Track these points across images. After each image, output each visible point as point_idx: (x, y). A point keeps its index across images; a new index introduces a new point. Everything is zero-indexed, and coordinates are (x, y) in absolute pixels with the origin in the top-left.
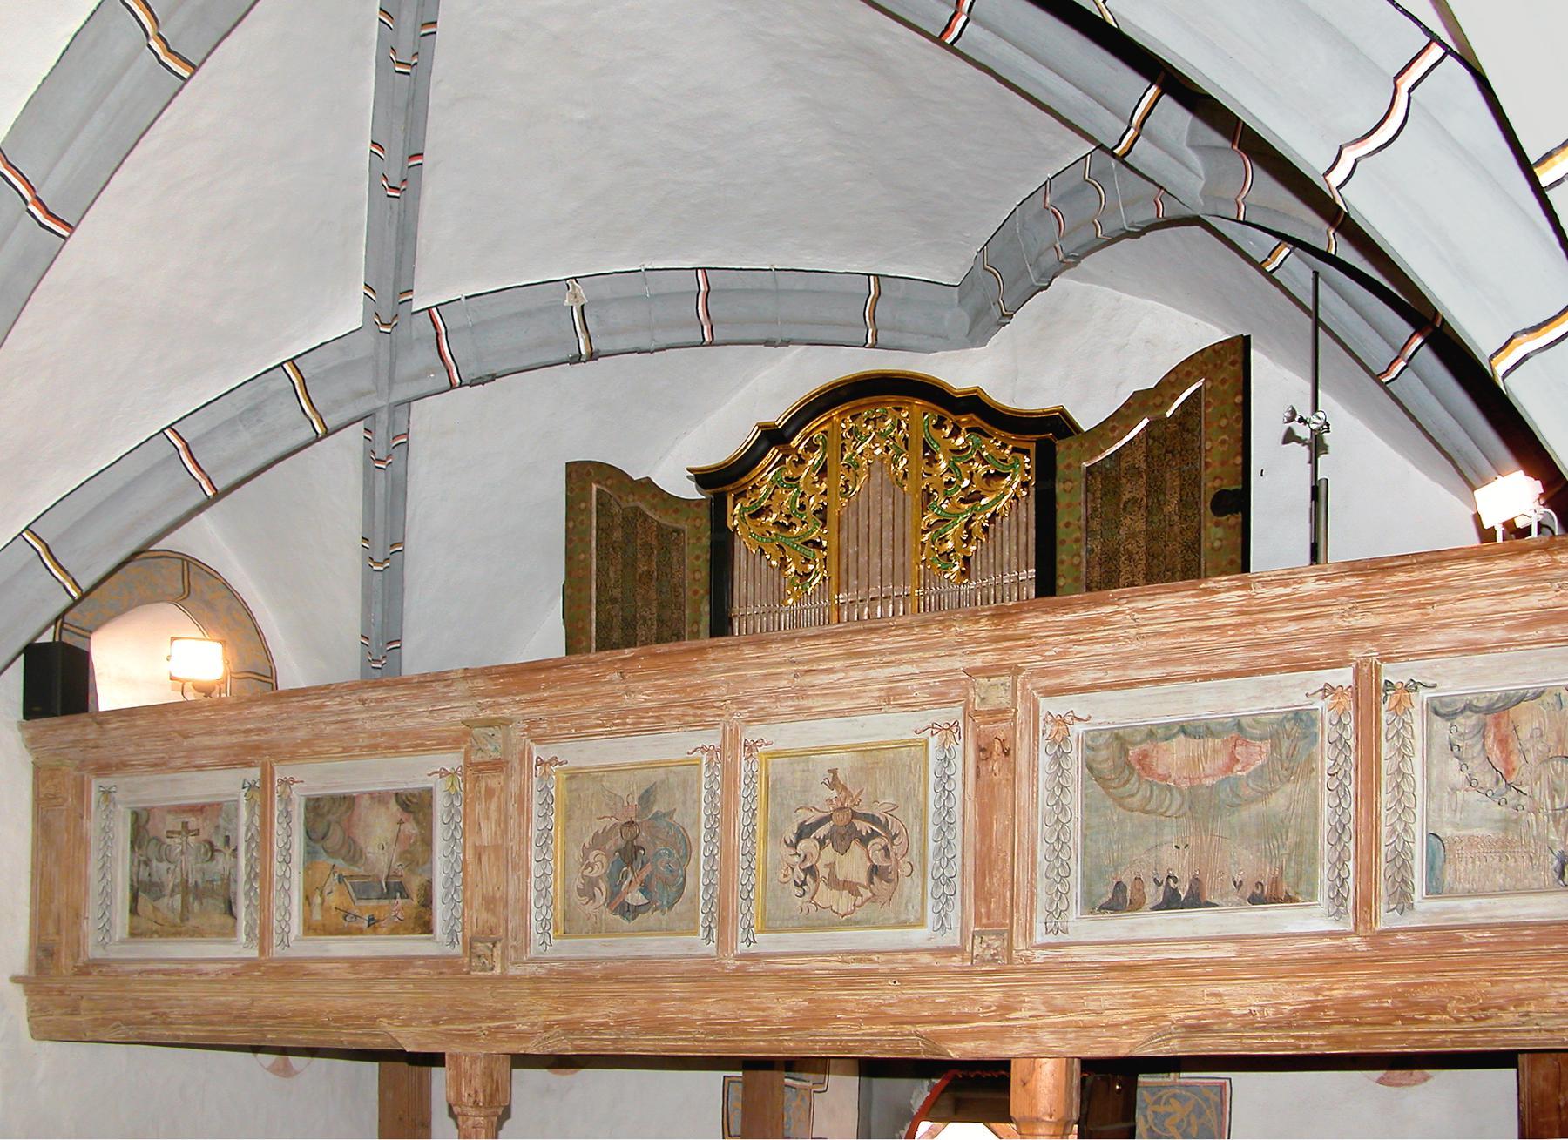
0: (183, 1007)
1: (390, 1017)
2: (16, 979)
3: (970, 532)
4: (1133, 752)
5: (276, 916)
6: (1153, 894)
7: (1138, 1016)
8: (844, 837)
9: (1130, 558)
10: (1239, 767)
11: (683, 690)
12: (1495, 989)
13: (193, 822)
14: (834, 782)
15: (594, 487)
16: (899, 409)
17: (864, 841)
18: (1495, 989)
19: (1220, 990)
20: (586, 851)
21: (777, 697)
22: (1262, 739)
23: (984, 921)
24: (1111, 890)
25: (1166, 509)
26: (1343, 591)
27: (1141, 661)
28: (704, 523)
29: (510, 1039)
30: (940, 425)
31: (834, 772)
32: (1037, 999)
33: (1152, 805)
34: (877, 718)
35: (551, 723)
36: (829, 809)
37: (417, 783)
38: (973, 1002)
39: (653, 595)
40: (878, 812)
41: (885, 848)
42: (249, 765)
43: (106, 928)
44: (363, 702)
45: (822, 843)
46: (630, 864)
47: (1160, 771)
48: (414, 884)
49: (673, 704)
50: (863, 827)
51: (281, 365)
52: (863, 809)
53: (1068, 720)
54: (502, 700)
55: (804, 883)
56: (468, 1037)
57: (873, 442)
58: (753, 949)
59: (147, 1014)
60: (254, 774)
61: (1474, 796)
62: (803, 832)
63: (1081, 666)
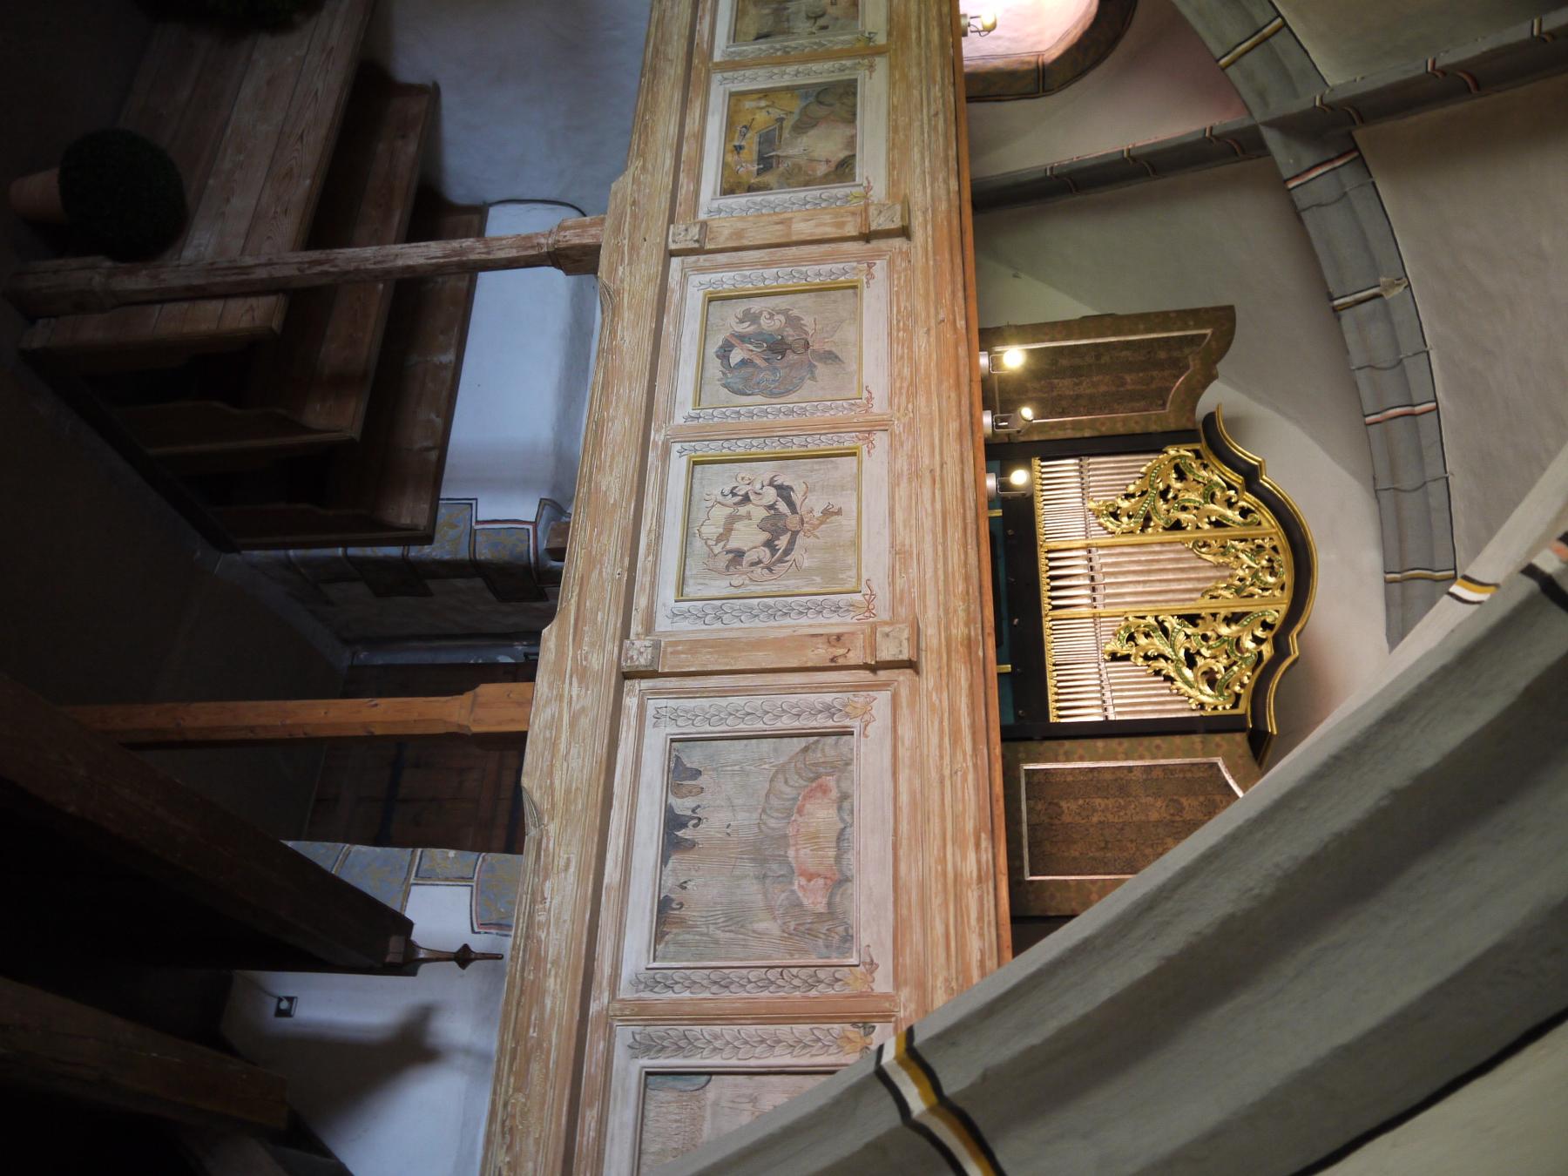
1: (644, 168)
3: (1155, 658)
4: (831, 781)
5: (748, 73)
6: (683, 806)
7: (557, 794)
8: (774, 527)
9: (1120, 808)
10: (803, 881)
11: (928, 376)
12: (531, 1141)
14: (827, 513)
15: (1208, 331)
16: (1282, 588)
17: (769, 544)
18: (531, 1141)
19: (572, 870)
20: (785, 312)
21: (914, 457)
22: (830, 904)
27: (917, 782)
28: (1172, 426)
29: (610, 263)
30: (1266, 626)
31: (839, 512)
33: (775, 802)
34: (885, 543)
35: (905, 269)
36: (802, 510)
37: (861, 171)
38: (592, 645)
39: (1103, 389)
40: (794, 555)
41: (760, 562)
42: (889, 34)
44: (936, 114)
45: (771, 507)
48: (768, 178)
49: (915, 369)
50: (782, 542)
51: (1279, 15)
52: (800, 540)
53: (866, 717)
55: (734, 495)
56: (618, 230)
57: (1249, 567)
58: (674, 454)
60: (881, 39)
62: (784, 492)
63: (919, 729)
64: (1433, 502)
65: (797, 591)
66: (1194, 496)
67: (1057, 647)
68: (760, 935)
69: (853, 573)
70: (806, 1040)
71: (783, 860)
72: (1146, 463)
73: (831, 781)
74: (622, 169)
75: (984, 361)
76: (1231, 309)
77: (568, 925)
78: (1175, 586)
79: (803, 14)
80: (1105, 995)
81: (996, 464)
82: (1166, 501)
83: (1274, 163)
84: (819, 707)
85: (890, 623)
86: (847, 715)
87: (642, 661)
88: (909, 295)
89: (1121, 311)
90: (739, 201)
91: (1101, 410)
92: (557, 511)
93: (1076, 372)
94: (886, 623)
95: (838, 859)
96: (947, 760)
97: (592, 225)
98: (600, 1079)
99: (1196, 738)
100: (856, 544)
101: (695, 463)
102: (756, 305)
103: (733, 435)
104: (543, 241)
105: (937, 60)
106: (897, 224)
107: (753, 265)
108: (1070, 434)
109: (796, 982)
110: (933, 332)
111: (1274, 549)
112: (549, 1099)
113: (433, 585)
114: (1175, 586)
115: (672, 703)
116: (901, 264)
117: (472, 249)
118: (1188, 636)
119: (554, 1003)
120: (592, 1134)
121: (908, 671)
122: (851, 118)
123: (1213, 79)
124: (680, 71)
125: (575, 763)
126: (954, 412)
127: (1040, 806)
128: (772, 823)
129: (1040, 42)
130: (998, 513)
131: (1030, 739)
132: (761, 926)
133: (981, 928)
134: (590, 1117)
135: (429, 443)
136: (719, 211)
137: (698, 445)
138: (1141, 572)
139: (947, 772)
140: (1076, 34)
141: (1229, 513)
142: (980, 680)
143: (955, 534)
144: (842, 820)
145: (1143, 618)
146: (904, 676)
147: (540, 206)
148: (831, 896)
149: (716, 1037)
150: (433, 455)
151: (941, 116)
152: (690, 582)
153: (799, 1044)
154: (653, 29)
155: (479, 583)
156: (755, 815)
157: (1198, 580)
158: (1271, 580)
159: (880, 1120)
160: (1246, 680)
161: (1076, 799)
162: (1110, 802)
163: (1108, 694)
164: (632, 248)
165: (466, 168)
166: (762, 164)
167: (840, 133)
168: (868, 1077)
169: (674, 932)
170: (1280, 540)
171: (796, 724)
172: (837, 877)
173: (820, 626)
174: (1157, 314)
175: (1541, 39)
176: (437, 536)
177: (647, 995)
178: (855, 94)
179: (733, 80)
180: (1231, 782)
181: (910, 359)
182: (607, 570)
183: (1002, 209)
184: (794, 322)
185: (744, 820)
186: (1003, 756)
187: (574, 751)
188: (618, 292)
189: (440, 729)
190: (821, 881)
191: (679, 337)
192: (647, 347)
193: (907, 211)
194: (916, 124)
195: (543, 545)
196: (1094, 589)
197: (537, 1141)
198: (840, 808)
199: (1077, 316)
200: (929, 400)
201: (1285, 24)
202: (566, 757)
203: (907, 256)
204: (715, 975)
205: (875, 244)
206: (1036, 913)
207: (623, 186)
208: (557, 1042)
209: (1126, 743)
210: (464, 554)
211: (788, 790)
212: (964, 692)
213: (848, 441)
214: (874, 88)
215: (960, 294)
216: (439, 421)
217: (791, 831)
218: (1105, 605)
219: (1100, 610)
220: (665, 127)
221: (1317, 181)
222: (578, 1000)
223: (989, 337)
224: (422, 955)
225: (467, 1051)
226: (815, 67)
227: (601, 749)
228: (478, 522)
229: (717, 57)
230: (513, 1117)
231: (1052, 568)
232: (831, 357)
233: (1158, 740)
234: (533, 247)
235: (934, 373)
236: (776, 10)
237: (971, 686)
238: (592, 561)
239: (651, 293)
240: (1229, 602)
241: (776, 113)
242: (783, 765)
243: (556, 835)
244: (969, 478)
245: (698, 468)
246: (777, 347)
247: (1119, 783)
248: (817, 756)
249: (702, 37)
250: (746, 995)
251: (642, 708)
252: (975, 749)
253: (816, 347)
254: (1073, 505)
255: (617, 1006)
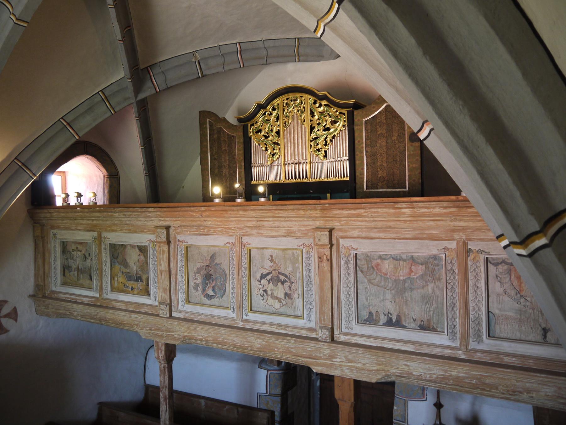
0: (77, 312)
1: (137, 325)
2: (30, 296)
3: (326, 142)
5: (104, 284)
6: (383, 319)
7: (378, 368)
8: (276, 281)
10: (413, 274)
11: (221, 221)
12: (518, 384)
13: (80, 247)
14: (272, 260)
15: (208, 120)
16: (302, 97)
17: (283, 283)
18: (518, 384)
19: (409, 364)
20: (195, 274)
21: (252, 228)
22: (422, 264)
23: (323, 322)
24: (368, 314)
25: (393, 138)
26: (451, 213)
27: (375, 230)
30: (315, 103)
31: (272, 256)
32: (342, 355)
33: (382, 284)
35: (182, 229)
36: (270, 270)
37: (144, 243)
38: (320, 352)
39: (227, 158)
41: (289, 286)
42: (94, 231)
43: (56, 284)
44: (125, 215)
45: (269, 282)
46: (208, 280)
47: (384, 271)
48: (144, 278)
50: (282, 278)
51: (98, 92)
52: (282, 271)
53: (350, 248)
54: (166, 219)
56: (160, 336)
57: (294, 108)
58: (247, 318)
59: (68, 313)
60: (95, 234)
61: (506, 298)
62: (263, 277)
64: (272, 45)
65: (301, 273)
66: (267, 127)
67: (321, 178)
68: (433, 291)
69: (295, 252)
70: (475, 274)
71: (405, 281)
72: (254, 143)
73: (374, 262)
74: (136, 333)
75: (217, 201)
76: (200, 112)
77: (431, 366)
78: (300, 134)
79: (84, 262)
80: (501, 166)
81: (253, 197)
82: (269, 136)
83: (150, 96)
84: (346, 266)
85: (315, 238)
86: (349, 255)
87: (327, 333)
88: (191, 227)
89: (199, 151)
90: (152, 289)
91: (235, 159)
92: (263, 362)
93: (220, 167)
94: (314, 241)
95: (404, 260)
96: (367, 219)
97: (158, 346)
98: (492, 355)
99: (356, 128)
100: (284, 250)
101: (251, 310)
102: (192, 284)
103: (241, 295)
104: (163, 366)
105: (105, 214)
106: (164, 231)
107: (176, 285)
108: (243, 170)
109: (452, 278)
110: (206, 219)
111: (287, 99)
112: (501, 376)
113: (290, 412)
114: (300, 134)
115: (343, 322)
116: (179, 230)
117: (164, 394)
118: (318, 130)
119: (462, 373)
120: (514, 359)
121: (333, 232)
122: (124, 246)
123: (118, 116)
124: (101, 310)
125: (367, 361)
126: (236, 212)
127: (380, 185)
128: (390, 285)
129: (100, 176)
130: (271, 197)
131: (355, 187)
132: (430, 290)
133: (432, 208)
134: (507, 360)
135: (236, 411)
136: (155, 297)
137: (244, 309)
138: (294, 146)
139: (372, 219)
140: (98, 163)
141: (274, 115)
142: (337, 206)
143: (282, 213)
144: (389, 258)
145: (311, 146)
146: (335, 234)
147: (147, 364)
148: (418, 263)
149: (474, 309)
150: (240, 410)
151: (126, 213)
152: (296, 313)
153: (476, 277)
154: (85, 319)
155: (289, 392)
156: (387, 291)
157: (298, 126)
158: (298, 100)
159: (549, 256)
160: (335, 110)
161: (378, 171)
162: (379, 159)
163: (339, 159)
164: (167, 331)
165: (131, 392)
166: (139, 281)
167: (129, 250)
168: (531, 260)
169: (433, 324)
170: (284, 97)
171: (352, 275)
172: (411, 261)
173: (315, 265)
174: (201, 138)
175: (115, 5)
176: (272, 409)
177: (458, 336)
178: (115, 244)
179: (106, 290)
180: (372, 116)
181: (215, 228)
182: (291, 346)
183: (158, 192)
184: (199, 270)
185: (389, 296)
186: (362, 198)
187: (362, 361)
188: (184, 337)
189: (352, 414)
190: (413, 267)
191: (202, 314)
192: (206, 327)
193: (160, 227)
194: (128, 222)
195: (276, 367)
196: (300, 163)
197: (518, 381)
198: (385, 259)
199: (199, 167)
200: (231, 221)
201: (101, 91)
202: (364, 364)
203: (177, 228)
204: (450, 309)
205: (171, 239)
206: (420, 187)
207: (143, 333)
208: (477, 372)
209: (357, 153)
210: (279, 399)
211: (377, 279)
212: (341, 212)
213: (245, 252)
214: (113, 237)
215: (192, 209)
216: (227, 407)
217: (393, 278)
218: (306, 159)
219: (308, 161)
220: (122, 316)
221: (157, 81)
222: (461, 363)
223: (207, 199)
224: (438, 423)
225: (473, 404)
226: (104, 259)
227: (360, 351)
228: (267, 393)
229: (97, 295)
230: (508, 391)
231: (292, 178)
232: (213, 257)
233: (356, 142)
234: (165, 369)
235: (221, 219)
236: (81, 273)
237: (339, 209)
238: (288, 351)
239: (185, 324)
240: (306, 115)
241: (120, 274)
242: (368, 280)
243: (395, 369)
244: (261, 207)
245: (253, 309)
246: (208, 277)
247: (372, 156)
248: (365, 268)
249: (89, 301)
250: (457, 297)
251: (345, 334)
252: (363, 209)
253: (209, 262)
254: (268, 169)
255: (462, 348)
